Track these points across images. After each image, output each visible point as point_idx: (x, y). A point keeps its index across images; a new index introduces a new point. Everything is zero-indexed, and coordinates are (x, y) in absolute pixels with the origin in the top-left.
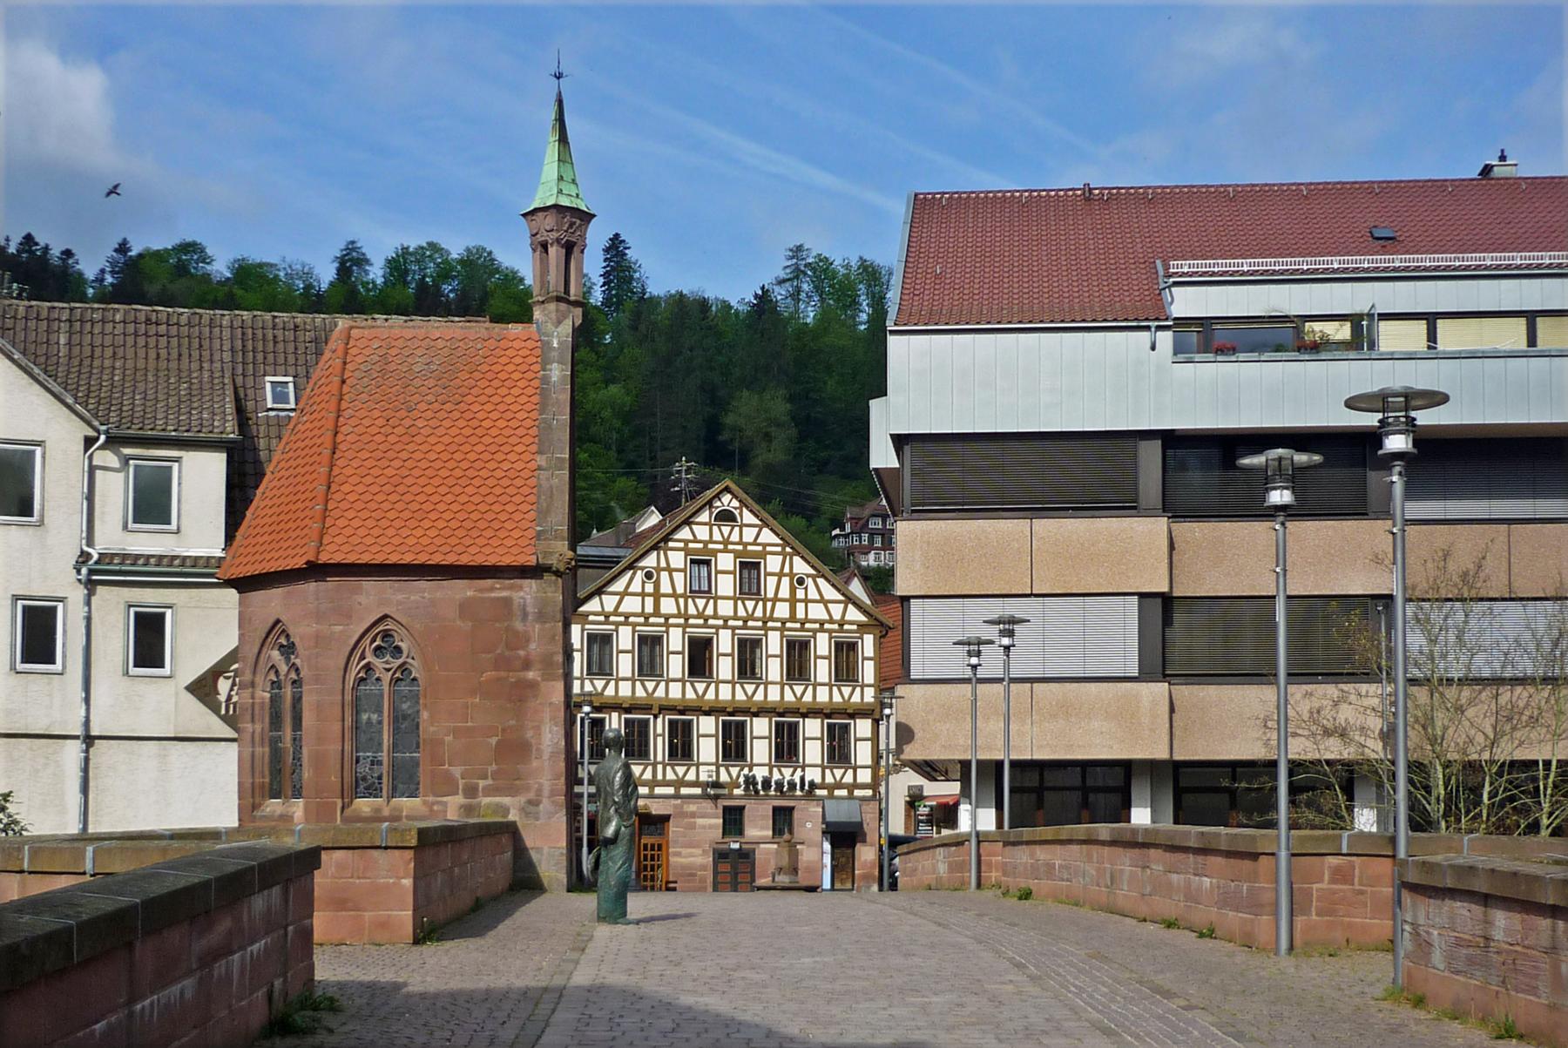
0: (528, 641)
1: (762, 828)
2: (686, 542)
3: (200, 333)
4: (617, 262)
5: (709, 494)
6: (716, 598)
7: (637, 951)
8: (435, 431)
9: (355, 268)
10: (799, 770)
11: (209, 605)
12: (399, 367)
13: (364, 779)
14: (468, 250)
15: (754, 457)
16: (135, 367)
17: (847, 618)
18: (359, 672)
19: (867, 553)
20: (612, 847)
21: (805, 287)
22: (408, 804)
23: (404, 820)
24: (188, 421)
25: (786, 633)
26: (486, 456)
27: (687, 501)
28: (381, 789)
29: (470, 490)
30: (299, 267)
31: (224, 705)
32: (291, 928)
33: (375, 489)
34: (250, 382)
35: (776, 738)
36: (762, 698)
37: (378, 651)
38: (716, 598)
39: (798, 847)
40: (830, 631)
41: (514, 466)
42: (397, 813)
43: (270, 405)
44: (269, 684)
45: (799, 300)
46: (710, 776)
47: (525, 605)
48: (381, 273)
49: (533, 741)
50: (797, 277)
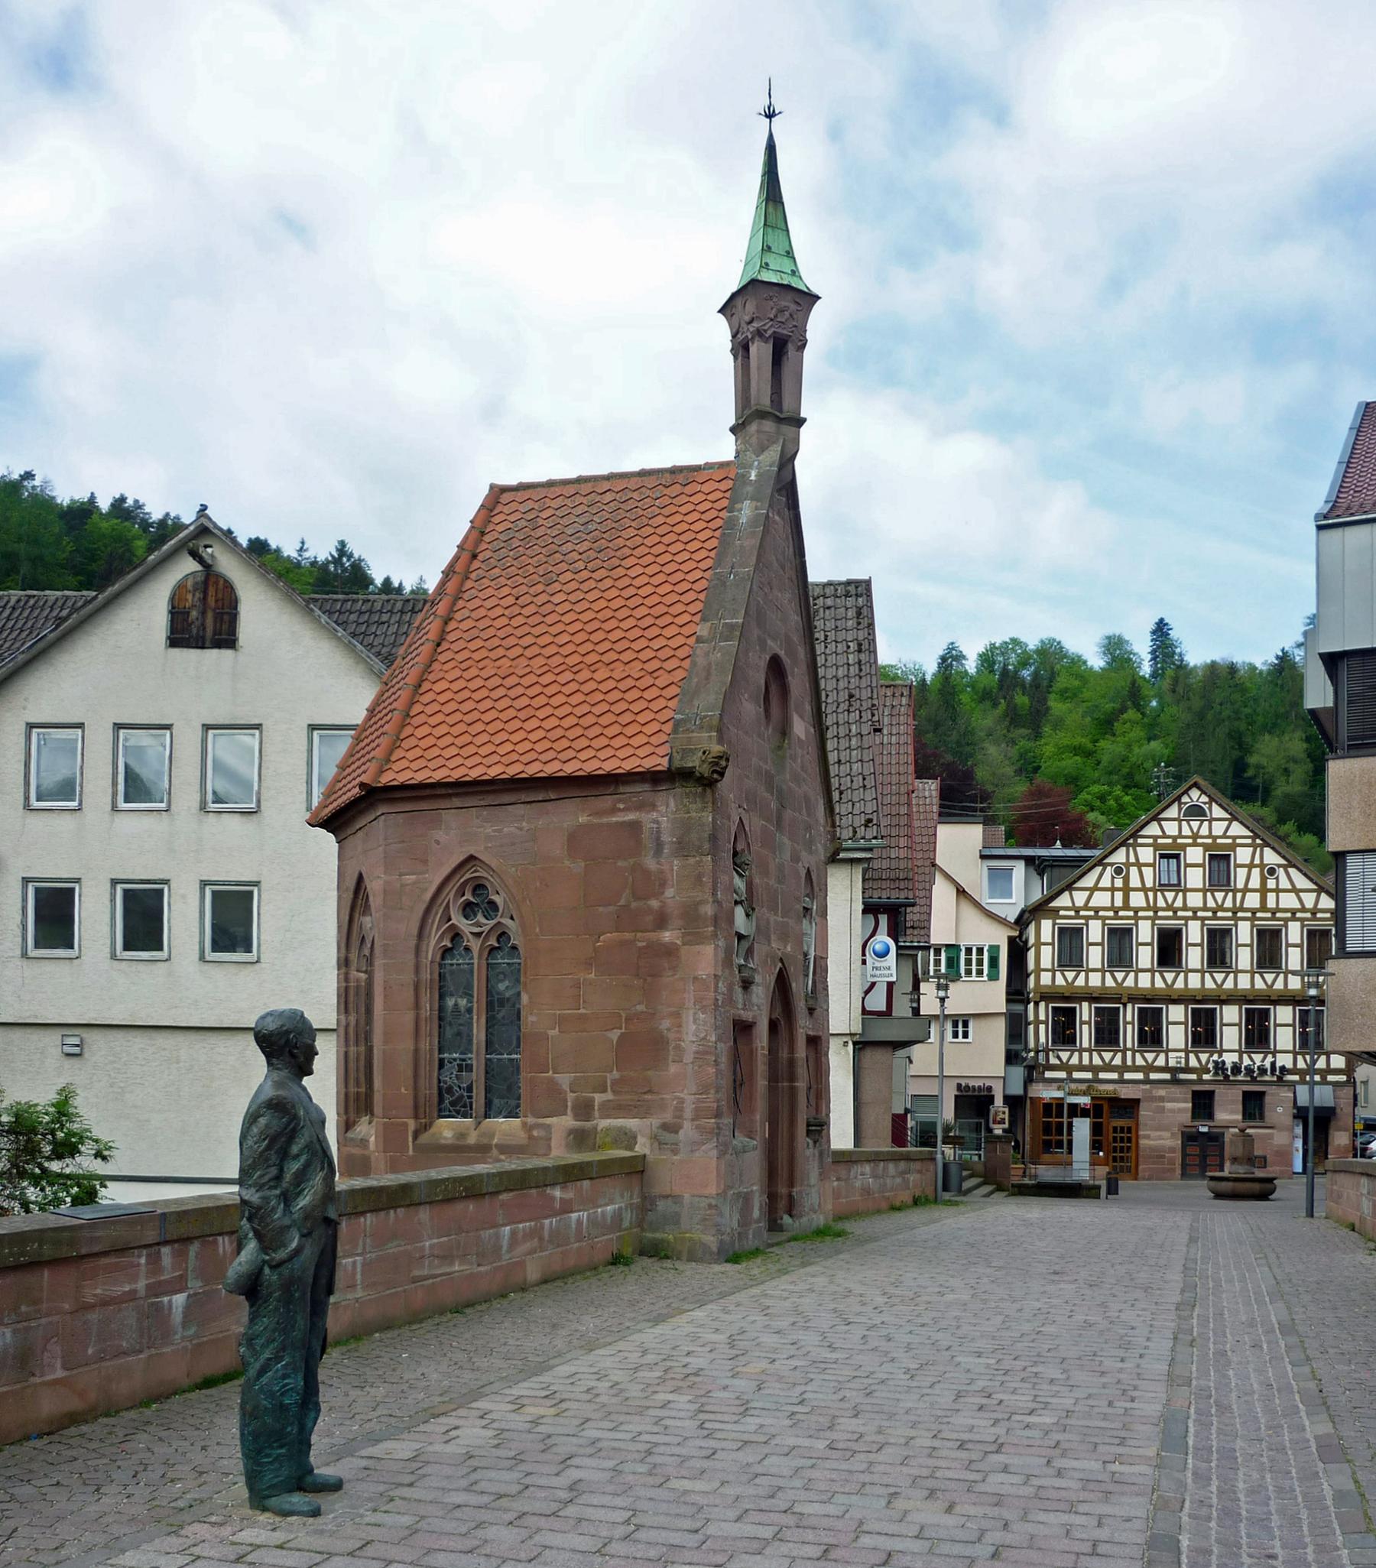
0: (663, 885)
1: (1232, 1112)
2: (1155, 838)
6: (1185, 891)
10: (1270, 1056)
14: (1042, 641)
17: (1319, 907)
18: (441, 938)
23: (495, 1152)
35: (1246, 1026)
38: (1185, 891)
40: (1302, 920)
42: (485, 1141)
46: (1178, 1062)
47: (659, 832)
49: (671, 1036)
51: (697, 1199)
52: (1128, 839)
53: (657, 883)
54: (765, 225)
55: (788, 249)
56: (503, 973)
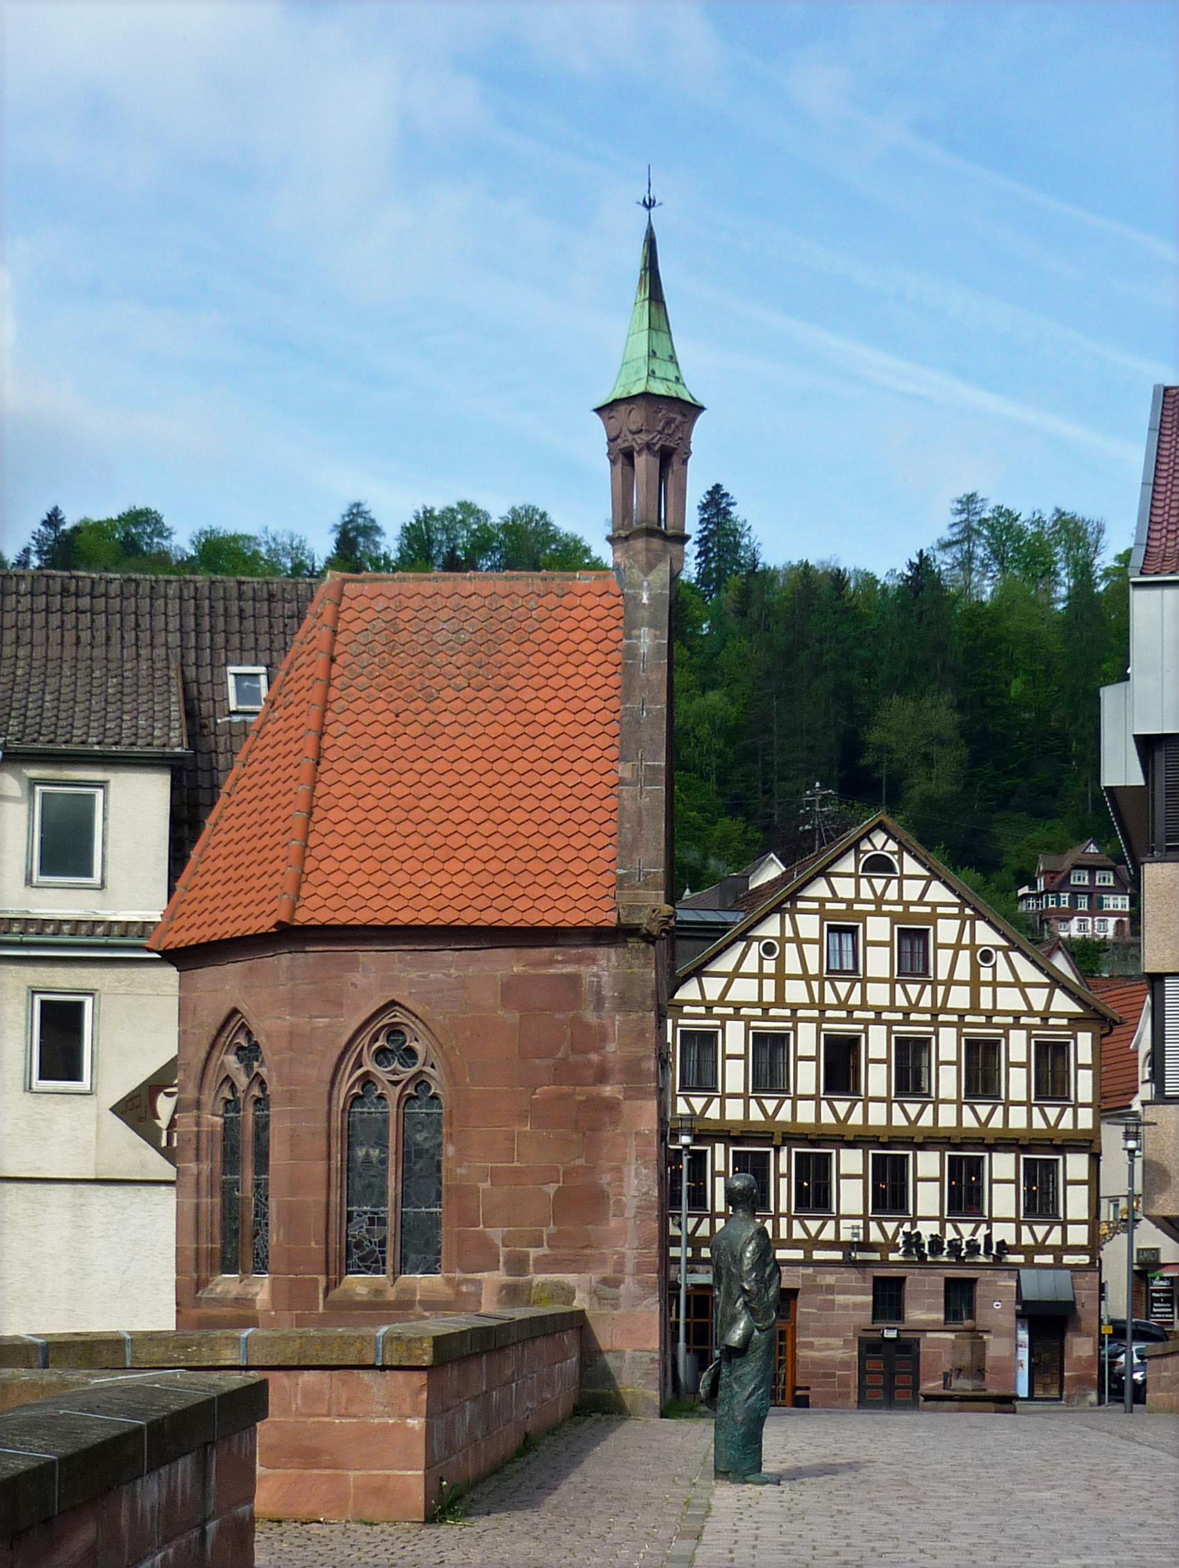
0: (604, 1038)
1: (930, 1309)
2: (822, 901)
3: (137, 607)
4: (717, 524)
5: (855, 832)
6: (865, 981)
7: (787, 1539)
8: (467, 730)
9: (361, 539)
10: (984, 1226)
11: (147, 991)
12: (414, 637)
13: (359, 1245)
15: (909, 788)
16: (46, 657)
19: (1067, 920)
20: (738, 1361)
21: (980, 552)
22: (424, 1283)
23: (418, 1309)
24: (117, 730)
25: (965, 1030)
26: (543, 766)
27: (823, 844)
28: (384, 1260)
29: (518, 816)
30: (287, 540)
31: (164, 1134)
32: (212, 1526)
33: (377, 815)
34: (206, 674)
36: (930, 1123)
37: (382, 1056)
38: (865, 981)
39: (986, 1337)
40: (1027, 1027)
41: (584, 779)
43: (233, 708)
44: (221, 1104)
45: (971, 570)
46: (856, 1235)
47: (599, 986)
48: (394, 545)
49: (611, 1191)
50: (968, 539)
51: (638, 1353)
52: (783, 902)
53: (598, 1037)
54: (650, 327)
55: (670, 353)
56: (419, 1123)
